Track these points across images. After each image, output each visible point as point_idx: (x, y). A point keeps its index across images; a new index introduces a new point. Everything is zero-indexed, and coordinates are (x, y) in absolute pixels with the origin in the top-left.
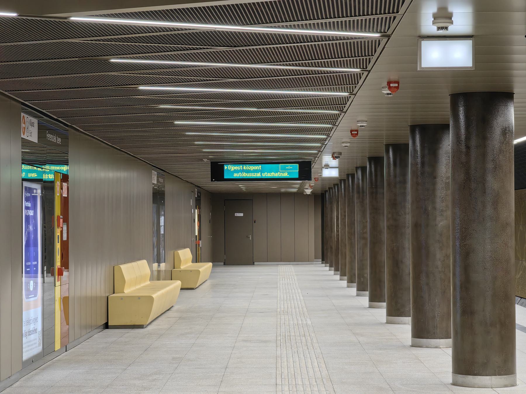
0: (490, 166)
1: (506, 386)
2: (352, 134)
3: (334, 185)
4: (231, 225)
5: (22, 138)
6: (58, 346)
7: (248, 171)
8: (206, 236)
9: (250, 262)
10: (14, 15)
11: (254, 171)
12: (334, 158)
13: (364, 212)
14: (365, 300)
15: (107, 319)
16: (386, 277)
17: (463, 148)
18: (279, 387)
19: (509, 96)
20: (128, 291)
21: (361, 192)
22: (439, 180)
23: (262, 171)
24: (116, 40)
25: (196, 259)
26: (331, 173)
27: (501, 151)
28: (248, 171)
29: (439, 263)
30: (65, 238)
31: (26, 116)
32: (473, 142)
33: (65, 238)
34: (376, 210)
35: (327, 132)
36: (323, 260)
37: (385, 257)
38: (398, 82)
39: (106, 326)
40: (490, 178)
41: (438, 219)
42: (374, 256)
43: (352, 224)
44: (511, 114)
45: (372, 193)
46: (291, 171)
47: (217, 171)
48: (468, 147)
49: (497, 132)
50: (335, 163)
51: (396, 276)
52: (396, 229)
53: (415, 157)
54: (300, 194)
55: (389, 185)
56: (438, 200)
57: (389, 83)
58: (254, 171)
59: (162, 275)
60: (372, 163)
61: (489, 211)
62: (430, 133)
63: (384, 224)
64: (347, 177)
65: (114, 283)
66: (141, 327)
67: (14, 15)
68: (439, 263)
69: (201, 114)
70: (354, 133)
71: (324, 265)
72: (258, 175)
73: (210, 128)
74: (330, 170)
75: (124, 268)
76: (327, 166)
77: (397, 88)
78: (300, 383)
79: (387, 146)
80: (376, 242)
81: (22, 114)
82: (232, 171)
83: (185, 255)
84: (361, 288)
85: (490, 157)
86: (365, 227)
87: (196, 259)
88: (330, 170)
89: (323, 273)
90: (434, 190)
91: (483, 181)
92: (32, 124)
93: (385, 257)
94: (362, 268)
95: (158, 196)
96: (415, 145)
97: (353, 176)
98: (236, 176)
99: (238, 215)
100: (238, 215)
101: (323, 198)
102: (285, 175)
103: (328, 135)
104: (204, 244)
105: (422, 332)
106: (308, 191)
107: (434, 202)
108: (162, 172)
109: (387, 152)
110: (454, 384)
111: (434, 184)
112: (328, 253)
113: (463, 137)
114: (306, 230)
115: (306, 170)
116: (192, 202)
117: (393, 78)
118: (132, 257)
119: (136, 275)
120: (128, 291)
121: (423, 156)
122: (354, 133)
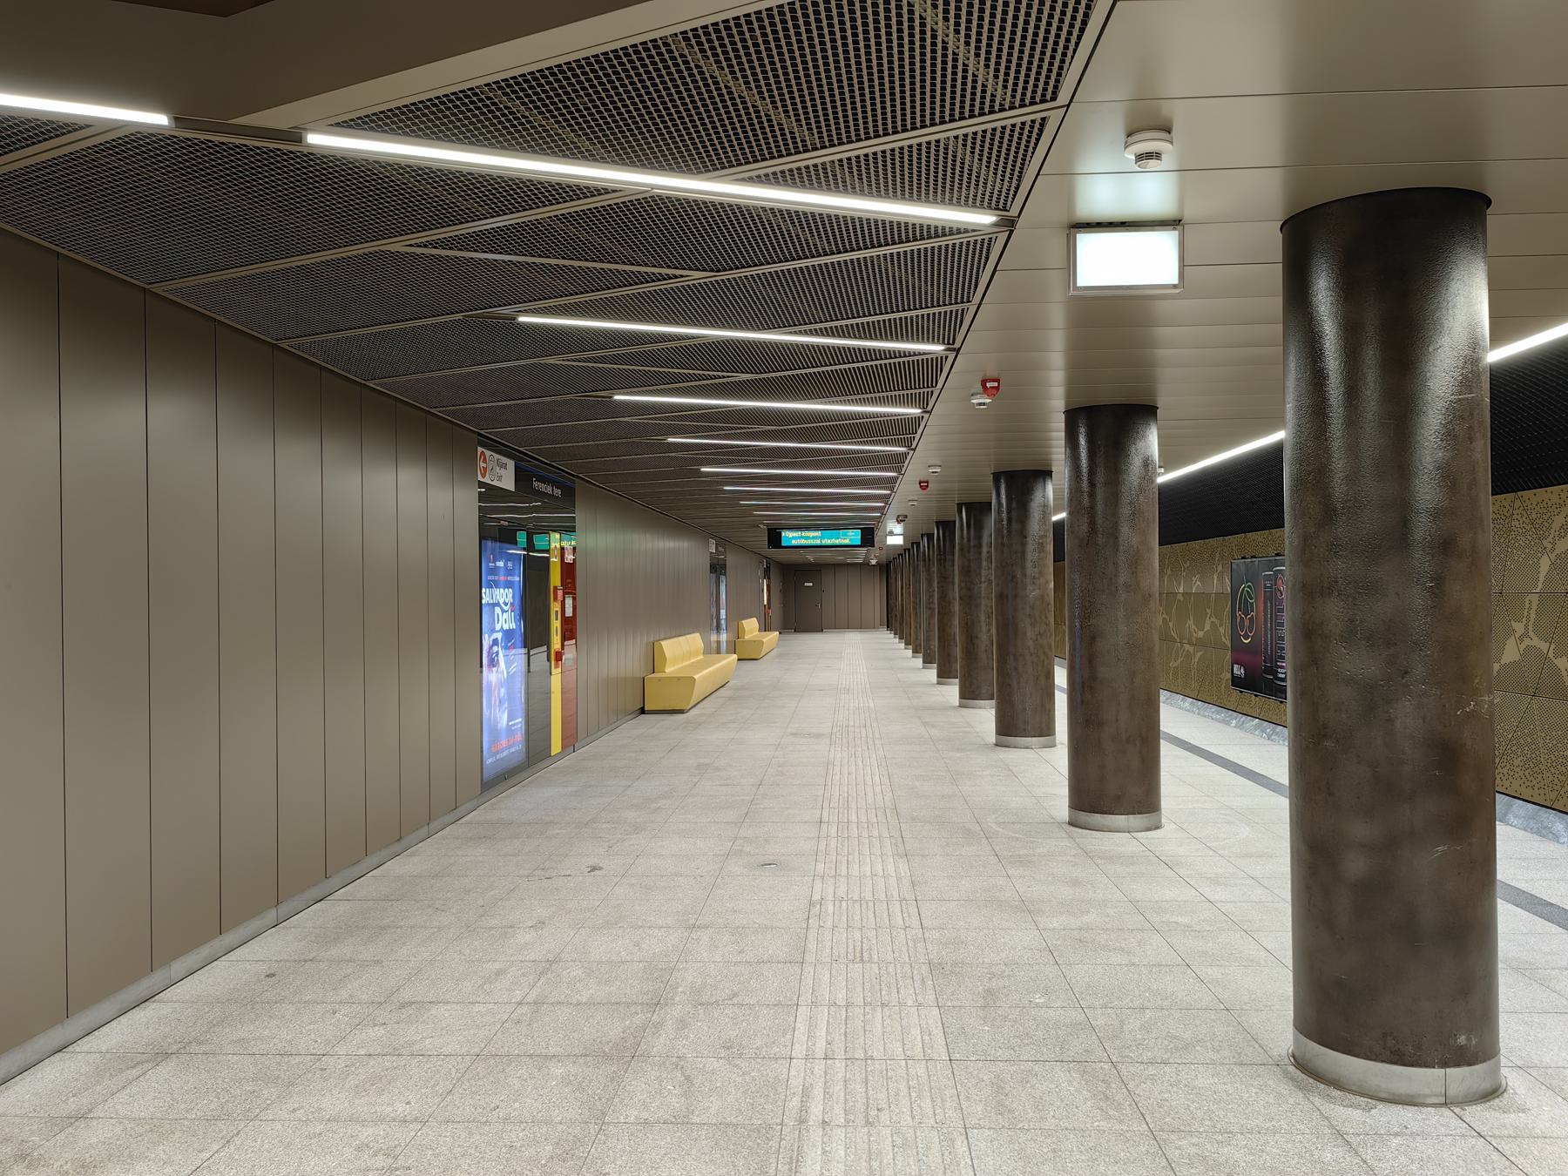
0: (1125, 511)
1: (1149, 829)
3: (903, 552)
4: (802, 595)
6: (556, 747)
7: (807, 538)
8: (776, 605)
9: (819, 629)
10: (158, 119)
11: (812, 538)
12: (899, 522)
13: (930, 581)
14: (932, 674)
15: (641, 704)
16: (958, 651)
17: (1085, 485)
18: (824, 826)
20: (670, 670)
21: (927, 560)
22: (1030, 540)
23: (821, 538)
25: (766, 627)
26: (896, 540)
27: (1141, 489)
28: (807, 538)
29: (1030, 643)
30: (569, 612)
31: (488, 453)
32: (1100, 478)
33: (569, 612)
34: (945, 579)
35: (890, 483)
37: (956, 627)
38: (998, 381)
39: (643, 711)
40: (1125, 529)
41: (1030, 587)
42: (943, 627)
43: (917, 594)
44: (1151, 442)
45: (939, 560)
46: (853, 537)
47: (774, 538)
48: (1092, 484)
49: (1136, 464)
50: (898, 529)
51: (970, 653)
52: (969, 599)
53: (999, 512)
54: (865, 565)
55: (961, 549)
56: (1029, 565)
57: (984, 383)
58: (812, 538)
59: (724, 646)
61: (1123, 578)
63: (956, 591)
64: (911, 547)
65: (653, 660)
66: (681, 712)
67: (158, 119)
68: (1030, 643)
69: (732, 453)
70: (924, 485)
72: (818, 542)
73: (732, 453)
74: (895, 536)
75: (667, 645)
76: (891, 533)
77: (997, 388)
78: (854, 819)
79: (960, 506)
80: (945, 614)
81: (480, 449)
82: (790, 537)
83: (751, 626)
84: (927, 661)
85: (1125, 499)
86: (931, 597)
87: (766, 627)
88: (895, 536)
89: (888, 641)
90: (1024, 552)
91: (1114, 534)
92: (504, 466)
93: (956, 627)
94: (928, 639)
95: (717, 568)
96: (1000, 499)
97: (918, 544)
98: (794, 543)
101: (888, 568)
102: (847, 542)
103: (892, 489)
104: (775, 614)
106: (874, 562)
107: (1024, 568)
108: (722, 542)
109: (960, 512)
110: (1071, 823)
111: (1024, 545)
112: (894, 621)
113: (1085, 470)
114: (873, 598)
115: (868, 537)
116: (760, 573)
117: (991, 373)
118: (680, 627)
119: (682, 652)
120: (670, 670)
121: (1009, 511)
122: (924, 485)
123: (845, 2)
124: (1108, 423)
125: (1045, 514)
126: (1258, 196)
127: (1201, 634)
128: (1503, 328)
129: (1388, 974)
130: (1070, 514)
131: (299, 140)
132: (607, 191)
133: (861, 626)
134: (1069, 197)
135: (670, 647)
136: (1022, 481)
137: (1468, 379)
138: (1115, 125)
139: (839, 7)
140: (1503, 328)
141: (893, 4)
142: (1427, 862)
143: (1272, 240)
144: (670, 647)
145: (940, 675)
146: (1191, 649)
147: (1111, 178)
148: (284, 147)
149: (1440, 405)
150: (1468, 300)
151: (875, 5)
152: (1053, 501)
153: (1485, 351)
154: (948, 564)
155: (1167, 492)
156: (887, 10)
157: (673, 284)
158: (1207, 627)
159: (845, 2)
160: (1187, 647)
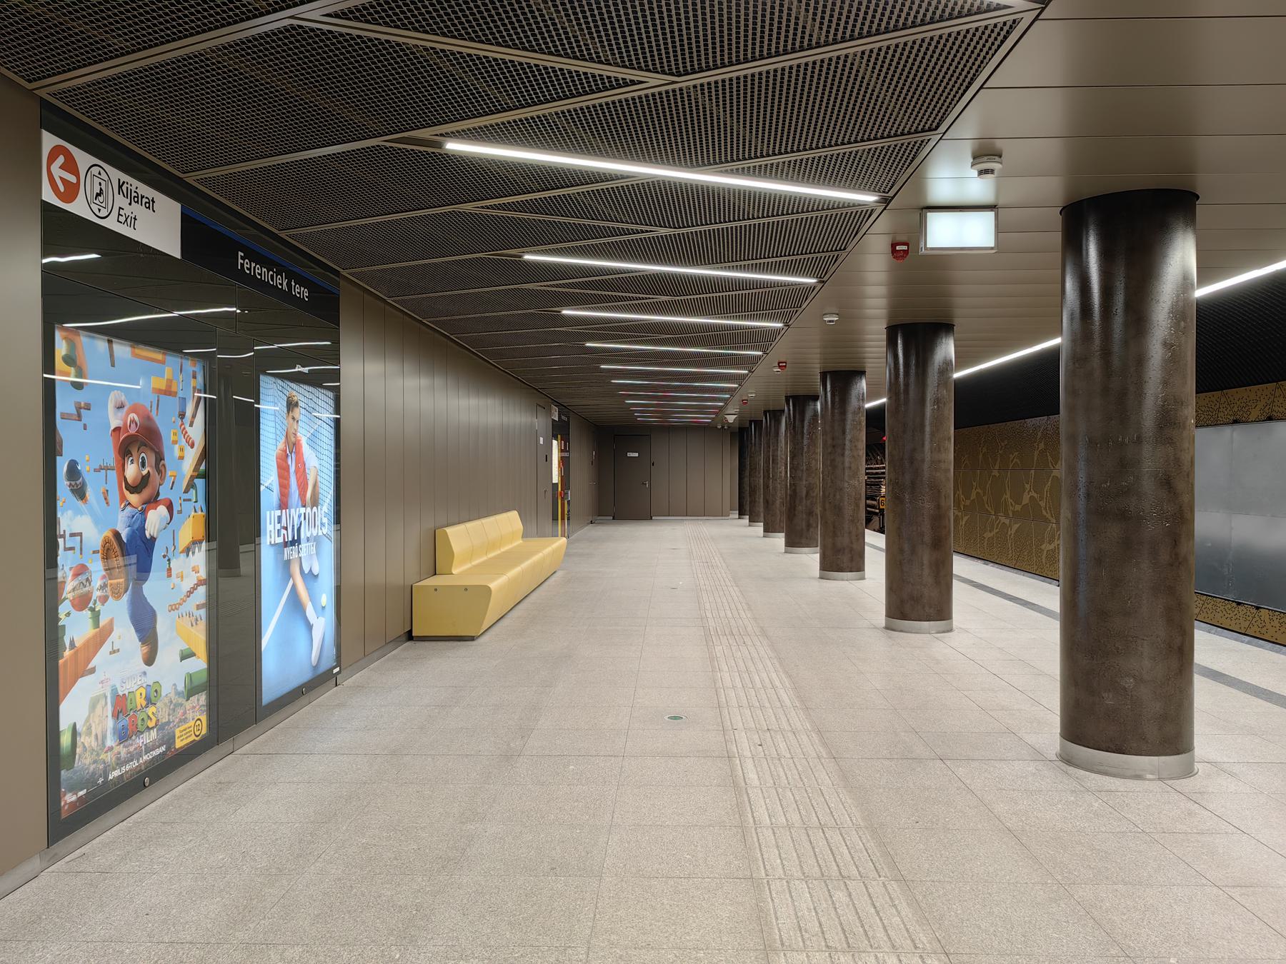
2: (894, 251)
5: (47, 207)
19: (862, 373)
24: (557, 286)
36: (741, 514)
39: (410, 636)
44: (947, 349)
60: (913, 352)
62: (775, 414)
66: (472, 639)
71: (746, 520)
73: (628, 355)
79: (765, 413)
81: (49, 141)
85: (849, 416)
96: (826, 393)
99: (631, 455)
100: (631, 455)
105: (768, 530)
112: (747, 504)
114: (721, 474)
122: (782, 365)
123: (672, 1)
124: (916, 333)
125: (946, 368)
126: (1047, 190)
127: (1018, 508)
128: (1207, 271)
129: (1121, 703)
130: (890, 398)
131: (440, 145)
132: (628, 177)
133: (721, 513)
134: (921, 188)
135: (459, 536)
136: (842, 378)
137: (1178, 314)
138: (967, 149)
139: (668, 5)
140: (1207, 271)
141: (708, 3)
142: (1144, 662)
143: (1055, 218)
144: (459, 536)
145: (765, 531)
146: (1007, 522)
147: (950, 175)
148: (430, 150)
149: (1166, 310)
150: (1182, 255)
151: (694, 4)
152: (869, 396)
153: (1193, 288)
154: (799, 437)
155: (959, 384)
156: (703, 8)
157: (650, 235)
158: (1026, 500)
159: (672, 1)
160: (1003, 519)
